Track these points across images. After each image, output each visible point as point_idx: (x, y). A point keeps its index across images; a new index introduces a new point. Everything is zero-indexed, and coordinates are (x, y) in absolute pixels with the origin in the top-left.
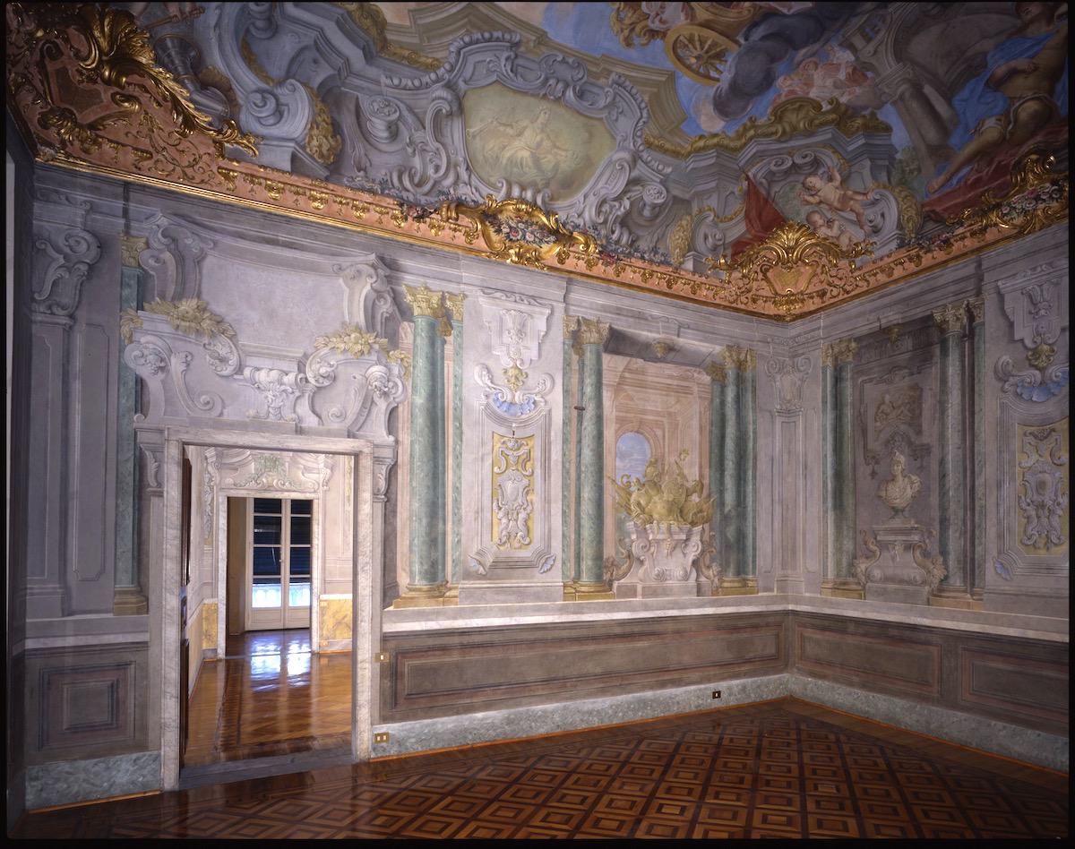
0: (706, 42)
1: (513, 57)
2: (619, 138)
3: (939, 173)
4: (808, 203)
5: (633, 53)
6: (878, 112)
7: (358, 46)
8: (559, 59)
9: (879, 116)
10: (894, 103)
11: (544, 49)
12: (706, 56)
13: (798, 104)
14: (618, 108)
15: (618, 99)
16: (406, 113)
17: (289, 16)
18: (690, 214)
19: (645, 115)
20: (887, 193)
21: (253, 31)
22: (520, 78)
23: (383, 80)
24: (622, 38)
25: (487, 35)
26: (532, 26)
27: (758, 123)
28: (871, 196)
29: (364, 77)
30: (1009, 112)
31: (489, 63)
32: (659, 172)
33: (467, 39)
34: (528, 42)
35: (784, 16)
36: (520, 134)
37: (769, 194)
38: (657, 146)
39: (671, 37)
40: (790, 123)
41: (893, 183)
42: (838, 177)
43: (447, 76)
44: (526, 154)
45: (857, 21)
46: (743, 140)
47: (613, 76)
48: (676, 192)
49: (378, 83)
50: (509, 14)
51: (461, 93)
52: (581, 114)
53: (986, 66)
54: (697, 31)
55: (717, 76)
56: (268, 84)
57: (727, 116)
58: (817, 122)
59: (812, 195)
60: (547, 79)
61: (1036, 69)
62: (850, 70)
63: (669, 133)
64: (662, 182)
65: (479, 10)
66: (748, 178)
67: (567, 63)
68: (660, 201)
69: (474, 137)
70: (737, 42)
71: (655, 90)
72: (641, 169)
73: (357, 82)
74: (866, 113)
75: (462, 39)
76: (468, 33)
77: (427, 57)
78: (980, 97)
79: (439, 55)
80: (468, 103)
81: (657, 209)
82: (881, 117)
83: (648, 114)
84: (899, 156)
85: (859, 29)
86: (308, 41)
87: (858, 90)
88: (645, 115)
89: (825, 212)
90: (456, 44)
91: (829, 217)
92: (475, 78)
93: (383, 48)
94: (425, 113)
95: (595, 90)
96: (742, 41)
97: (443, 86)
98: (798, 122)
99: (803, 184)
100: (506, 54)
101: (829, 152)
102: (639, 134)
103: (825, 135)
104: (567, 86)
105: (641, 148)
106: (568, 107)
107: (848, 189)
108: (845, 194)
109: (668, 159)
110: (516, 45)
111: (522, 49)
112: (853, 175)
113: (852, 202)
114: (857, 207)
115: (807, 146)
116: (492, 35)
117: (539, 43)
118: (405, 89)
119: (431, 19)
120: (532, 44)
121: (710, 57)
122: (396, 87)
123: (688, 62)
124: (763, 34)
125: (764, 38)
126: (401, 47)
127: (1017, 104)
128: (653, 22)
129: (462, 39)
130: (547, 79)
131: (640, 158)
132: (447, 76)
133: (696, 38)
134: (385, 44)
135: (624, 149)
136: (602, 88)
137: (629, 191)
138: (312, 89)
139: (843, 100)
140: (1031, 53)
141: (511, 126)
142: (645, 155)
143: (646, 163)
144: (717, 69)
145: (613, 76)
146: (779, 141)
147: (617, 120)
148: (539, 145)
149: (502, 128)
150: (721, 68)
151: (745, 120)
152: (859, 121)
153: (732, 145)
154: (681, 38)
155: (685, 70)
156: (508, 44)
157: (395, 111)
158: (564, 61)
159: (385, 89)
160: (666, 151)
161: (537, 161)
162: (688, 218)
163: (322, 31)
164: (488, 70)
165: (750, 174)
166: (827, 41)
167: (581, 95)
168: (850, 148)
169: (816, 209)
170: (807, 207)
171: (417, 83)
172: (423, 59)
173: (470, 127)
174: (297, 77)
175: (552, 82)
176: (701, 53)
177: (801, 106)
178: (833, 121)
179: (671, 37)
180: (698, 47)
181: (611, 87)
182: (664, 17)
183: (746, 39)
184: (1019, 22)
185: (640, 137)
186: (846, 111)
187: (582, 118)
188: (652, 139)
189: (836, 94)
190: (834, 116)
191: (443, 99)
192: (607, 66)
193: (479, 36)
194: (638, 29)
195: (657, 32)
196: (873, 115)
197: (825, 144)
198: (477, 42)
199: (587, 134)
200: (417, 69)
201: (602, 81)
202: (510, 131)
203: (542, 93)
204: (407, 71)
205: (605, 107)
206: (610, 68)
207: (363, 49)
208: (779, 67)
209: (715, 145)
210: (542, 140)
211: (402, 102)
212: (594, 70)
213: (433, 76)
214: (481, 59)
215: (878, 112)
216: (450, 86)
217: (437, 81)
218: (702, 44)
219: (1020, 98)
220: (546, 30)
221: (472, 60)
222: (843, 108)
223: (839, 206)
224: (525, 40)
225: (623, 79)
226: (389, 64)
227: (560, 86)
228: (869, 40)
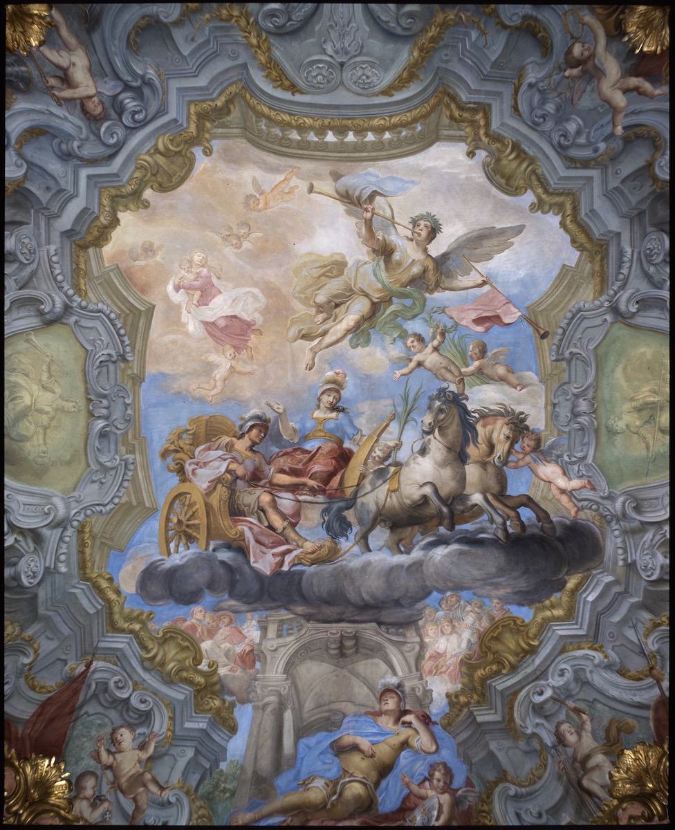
0: (196, 519)
1: (113, 359)
2: (76, 494)
3: (250, 809)
4: (97, 757)
5: (158, 463)
6: (238, 705)
7: (73, 225)
8: (128, 401)
9: (236, 710)
10: (255, 708)
11: (130, 382)
12: (184, 527)
13: (187, 644)
14: (105, 478)
15: (113, 472)
16: (29, 270)
17: (78, 174)
18: (22, 630)
19: (108, 508)
20: (185, 801)
21: (56, 141)
22: (97, 371)
23: (52, 248)
24: (166, 446)
25: (122, 332)
26: (144, 367)
27: (151, 625)
28: (167, 795)
29: (49, 231)
30: (338, 783)
31: (100, 340)
32: (57, 559)
33: (113, 316)
34: (130, 368)
35: (248, 562)
36: (45, 388)
37: (81, 706)
38: (83, 540)
39: (185, 487)
40: (165, 655)
41: (200, 793)
42: (151, 750)
43: (75, 304)
44: (27, 400)
45: (284, 614)
46: (126, 625)
47: (130, 457)
48: (42, 594)
49: (49, 242)
50: (146, 344)
51: (64, 321)
52: (86, 444)
53: (339, 727)
54: (200, 507)
55: (172, 551)
56: (16, 143)
57: (141, 590)
58: (185, 674)
59: (109, 752)
60: (105, 397)
61: (372, 756)
62: (248, 649)
63: (102, 543)
64: (47, 570)
65: (139, 319)
66: (88, 666)
67: (126, 409)
68: (25, 581)
69: (27, 341)
70: (208, 545)
71: (135, 504)
72: (52, 536)
73: (43, 224)
74: (229, 699)
75: (111, 312)
76: (118, 316)
77: (85, 285)
78: (321, 753)
79: (91, 295)
80: (57, 328)
81: (15, 584)
82: (237, 713)
83: (111, 510)
84: (223, 766)
85: (281, 621)
86: (63, 184)
87: (239, 673)
88: (108, 508)
89: (105, 781)
90: (105, 307)
91: (104, 792)
92: (83, 330)
93: (79, 246)
94: (35, 288)
95: (113, 447)
96: (211, 548)
97: (64, 302)
98: (172, 660)
99: (114, 731)
100: (113, 352)
101: (167, 713)
102: (89, 512)
103: (178, 694)
104: (107, 418)
105: (75, 523)
106: (88, 427)
107: (150, 771)
108: (142, 774)
109: (75, 558)
110: (123, 358)
111: (122, 365)
112: (166, 758)
113: (141, 789)
114: (143, 799)
115: (155, 693)
116: (124, 336)
117: (133, 378)
118: (51, 267)
119: (117, 284)
120: (129, 372)
121: (185, 531)
122: (50, 260)
123: (171, 517)
124: (226, 559)
125: (223, 563)
126: (86, 261)
127: (347, 779)
128: (190, 464)
129: (111, 312)
130: (105, 397)
131: (65, 529)
132: (75, 304)
133: (194, 509)
134: (84, 247)
135: (68, 507)
136: (116, 453)
137: (24, 536)
138: (24, 182)
139: (222, 671)
140: (375, 739)
141: (50, 376)
142: (70, 532)
143: (61, 539)
144: (177, 546)
145: (130, 457)
146: (142, 661)
147: (93, 482)
148: (40, 411)
149: (45, 368)
150: (181, 549)
151: (147, 609)
152: (217, 703)
153: (117, 617)
154: (188, 496)
155: (164, 519)
156: (122, 353)
157: (27, 260)
158: (126, 406)
159: (45, 248)
160: (82, 552)
161: (24, 414)
162: (17, 629)
163: (75, 195)
164: (94, 341)
165: (94, 663)
166: (254, 610)
167: (103, 435)
168: (188, 725)
169: (99, 772)
170: (92, 762)
171: (60, 278)
172: (82, 281)
173: (35, 336)
174: (30, 171)
175: (105, 402)
176: (185, 522)
177: (187, 647)
178: (199, 684)
179: (185, 487)
180: (188, 516)
181: (121, 460)
182: (199, 471)
183: (214, 550)
184: (377, 706)
185: (86, 516)
186: (215, 684)
187: (82, 445)
188: (87, 530)
189: (222, 660)
190: (202, 680)
191: (54, 305)
192: (137, 446)
193: (119, 326)
194: (179, 455)
195: (184, 472)
196: (232, 705)
197: (171, 705)
198: (114, 325)
199: (68, 458)
200: (72, 277)
201: (123, 449)
202: (45, 377)
203: (93, 397)
204: (68, 269)
205: (101, 464)
206: (137, 451)
207: (72, 230)
208: (209, 598)
209: (108, 601)
210: (47, 413)
211: (38, 265)
212: (130, 437)
213: (71, 292)
214: (102, 333)
215: (238, 705)
216: (67, 309)
217: (68, 297)
218: (192, 517)
219: (351, 775)
220: (146, 380)
221: (97, 324)
222: (215, 679)
223: (124, 786)
224: (130, 365)
225: (132, 467)
226: (67, 251)
227: (104, 412)
228: (279, 636)
